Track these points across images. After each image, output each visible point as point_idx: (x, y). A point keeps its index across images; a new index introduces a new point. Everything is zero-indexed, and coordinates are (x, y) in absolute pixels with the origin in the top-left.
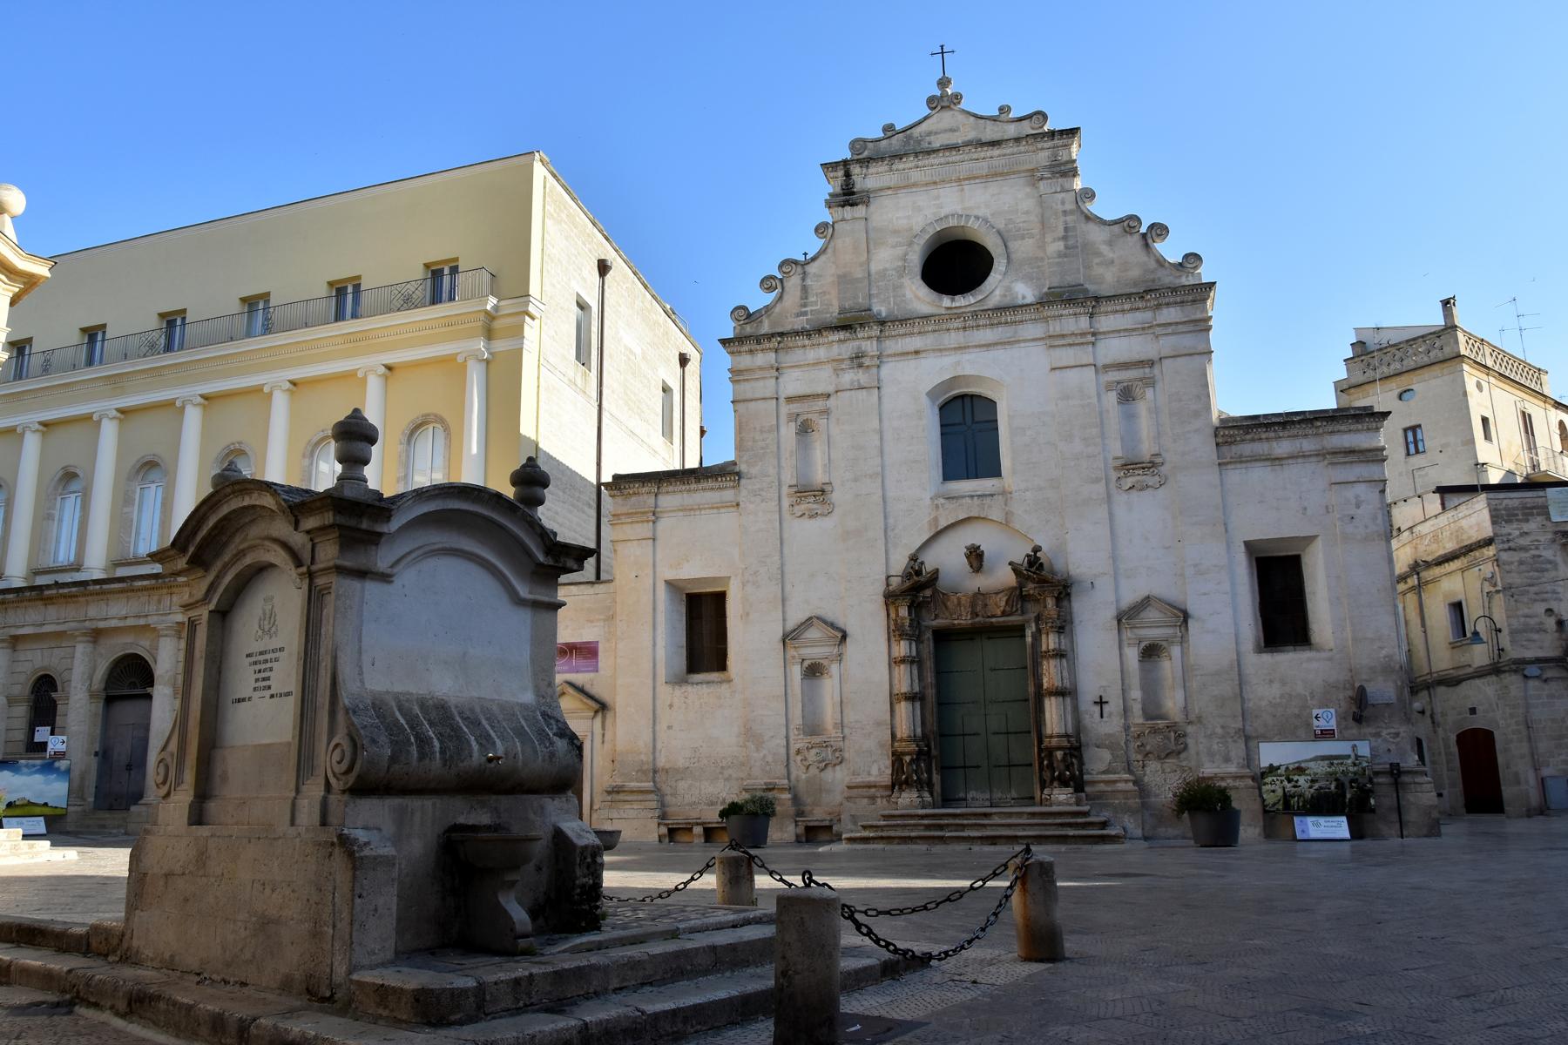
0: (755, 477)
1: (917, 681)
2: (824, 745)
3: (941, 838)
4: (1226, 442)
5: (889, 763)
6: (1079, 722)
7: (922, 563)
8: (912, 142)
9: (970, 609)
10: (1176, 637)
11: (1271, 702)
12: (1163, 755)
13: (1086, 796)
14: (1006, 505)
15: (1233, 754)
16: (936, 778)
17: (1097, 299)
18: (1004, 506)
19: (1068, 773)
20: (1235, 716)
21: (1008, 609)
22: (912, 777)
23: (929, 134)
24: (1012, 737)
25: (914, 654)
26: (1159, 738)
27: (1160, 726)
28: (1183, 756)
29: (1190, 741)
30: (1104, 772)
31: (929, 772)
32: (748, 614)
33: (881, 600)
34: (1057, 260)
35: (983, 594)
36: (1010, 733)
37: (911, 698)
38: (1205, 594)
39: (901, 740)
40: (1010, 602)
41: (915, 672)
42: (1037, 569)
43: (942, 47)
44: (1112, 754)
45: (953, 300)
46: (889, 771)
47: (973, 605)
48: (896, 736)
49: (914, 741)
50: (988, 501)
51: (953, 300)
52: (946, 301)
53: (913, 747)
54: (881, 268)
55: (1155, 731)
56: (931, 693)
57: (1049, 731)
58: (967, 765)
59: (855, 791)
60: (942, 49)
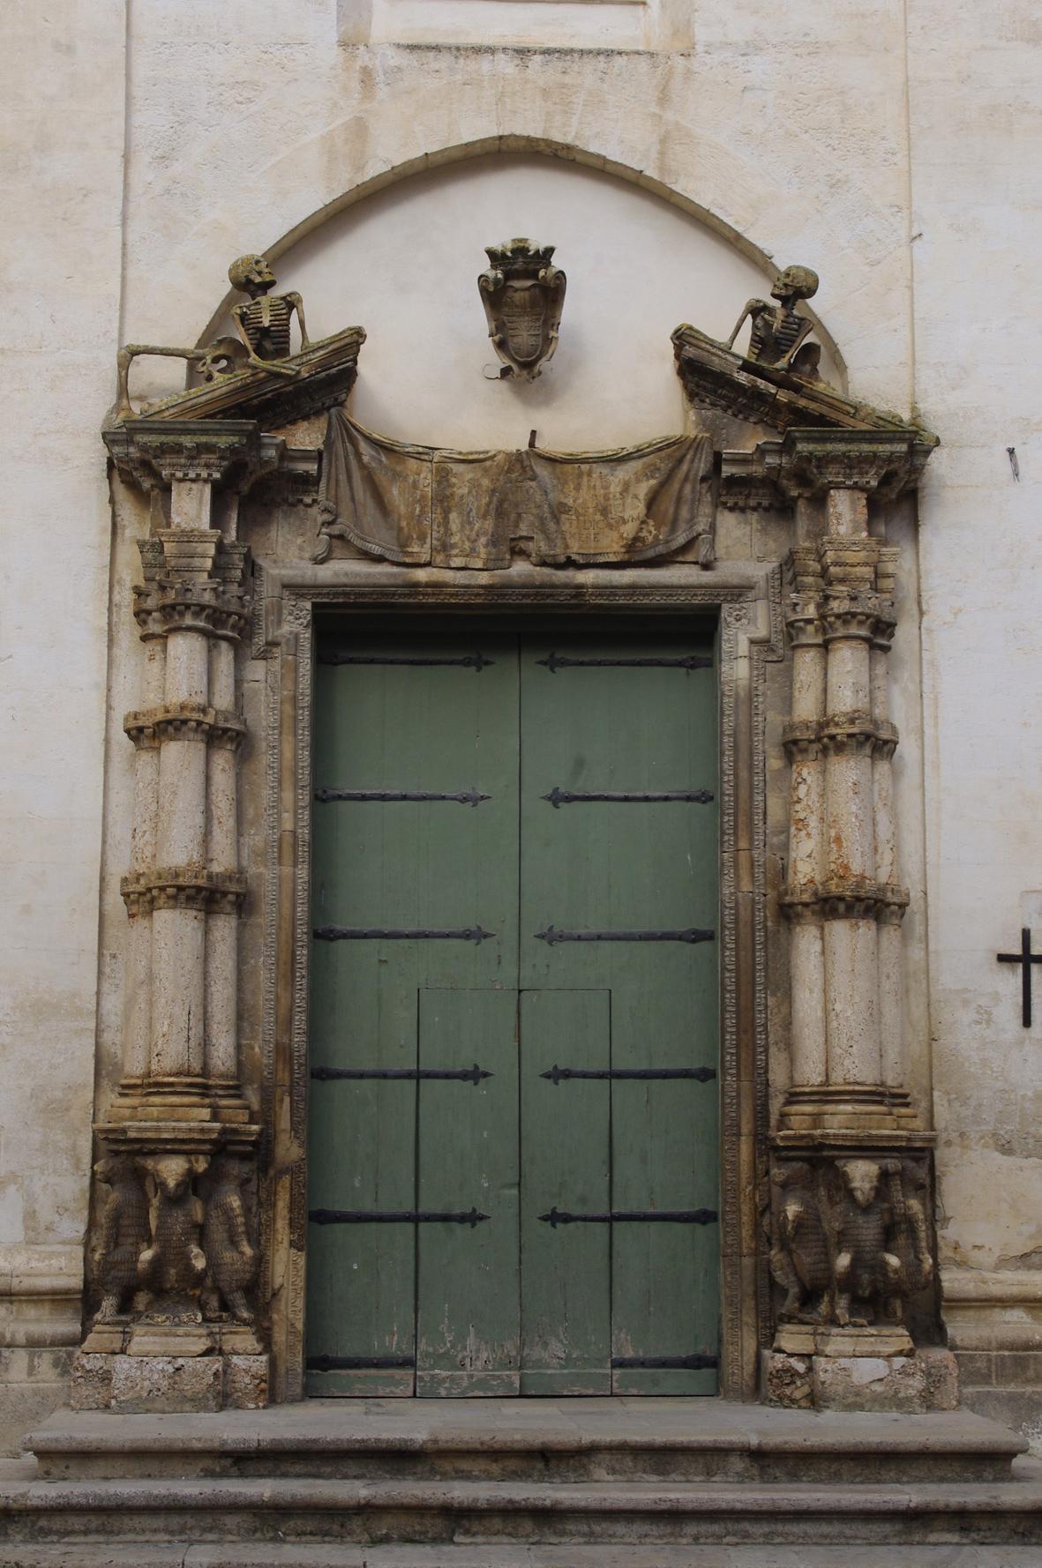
3: (548, 1517)
5: (74, 1186)
7: (291, 303)
9: (489, 524)
14: (663, 99)
16: (286, 1267)
18: (654, 109)
19: (893, 1260)
22: (186, 1259)
31: (259, 1236)
35: (552, 460)
36: (408, 1075)
41: (223, 780)
46: (74, 1227)
47: (502, 508)
49: (204, 1090)
50: (586, 75)
53: (196, 1118)
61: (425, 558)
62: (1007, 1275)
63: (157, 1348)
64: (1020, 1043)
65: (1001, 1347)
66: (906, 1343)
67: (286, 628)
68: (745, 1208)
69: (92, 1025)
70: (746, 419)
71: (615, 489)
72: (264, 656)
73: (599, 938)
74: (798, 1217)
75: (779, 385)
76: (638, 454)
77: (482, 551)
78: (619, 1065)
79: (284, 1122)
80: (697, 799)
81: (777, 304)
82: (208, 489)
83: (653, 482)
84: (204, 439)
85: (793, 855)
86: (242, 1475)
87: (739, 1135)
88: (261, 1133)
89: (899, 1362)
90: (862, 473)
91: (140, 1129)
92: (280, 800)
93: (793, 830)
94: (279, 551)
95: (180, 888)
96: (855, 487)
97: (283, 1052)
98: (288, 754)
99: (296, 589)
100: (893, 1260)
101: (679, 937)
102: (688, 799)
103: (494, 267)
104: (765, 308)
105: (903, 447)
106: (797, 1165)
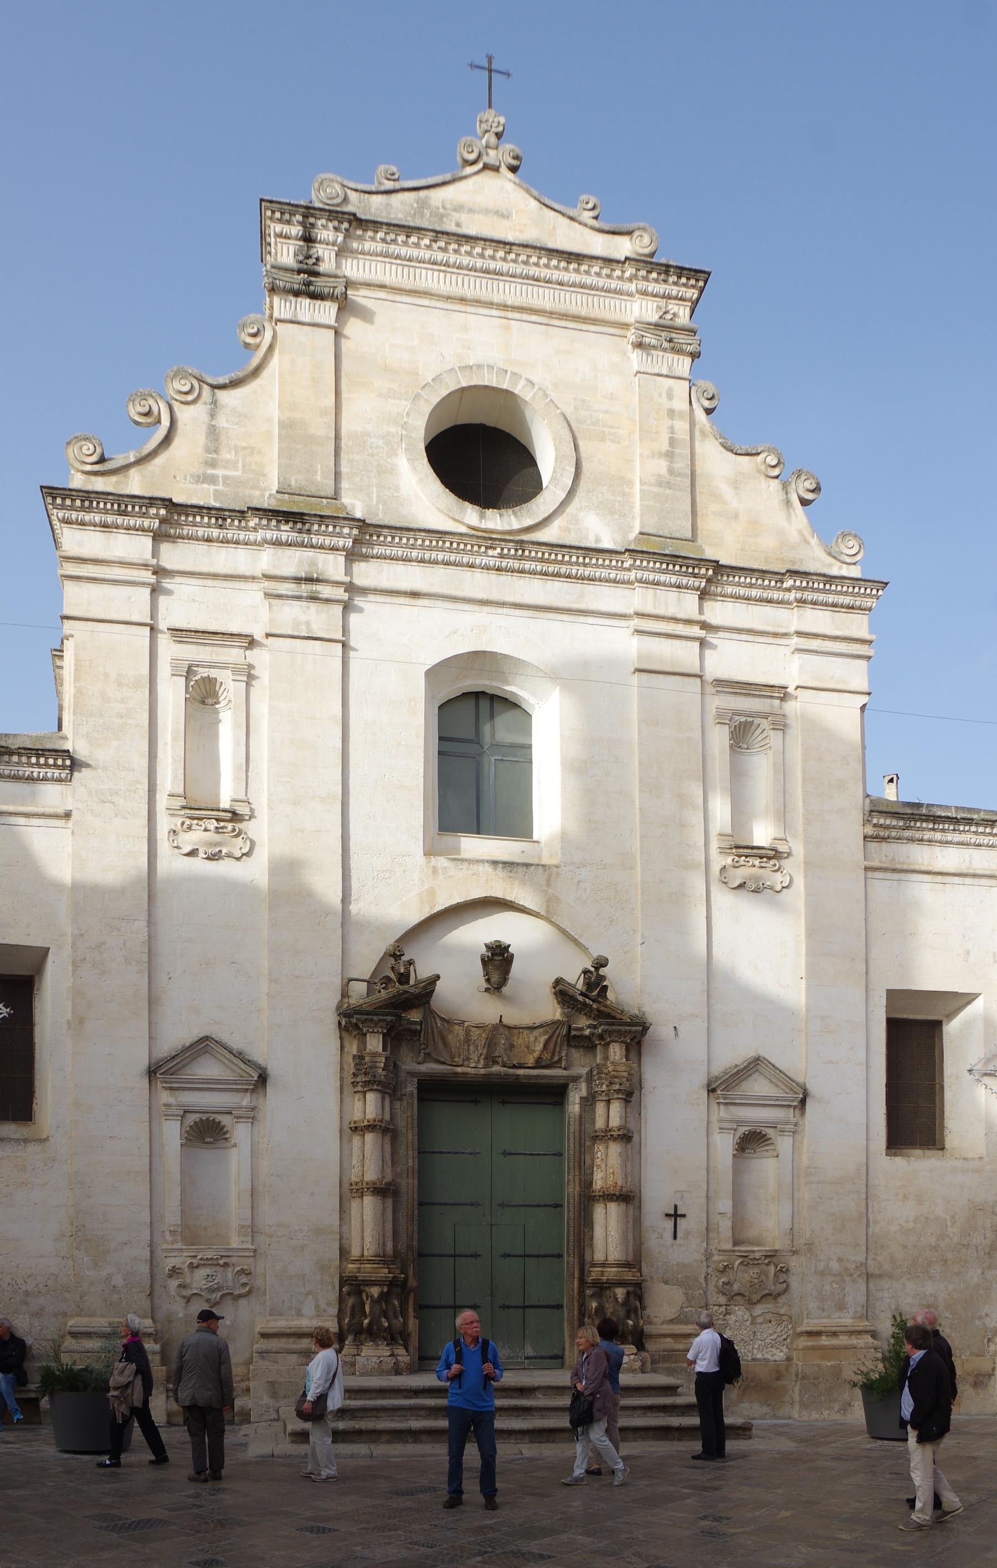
0: (105, 768)
1: (390, 1163)
2: (221, 1262)
4: (877, 837)
5: (333, 1296)
6: (641, 1244)
7: (411, 963)
8: (427, 213)
10: (787, 1123)
11: (902, 1227)
12: (756, 1297)
13: (652, 1356)
14: (548, 885)
15: (849, 1300)
16: (413, 1324)
17: (718, 567)
18: (545, 888)
19: (630, 1322)
20: (857, 1245)
21: (546, 1056)
23: (459, 208)
24: (531, 1263)
25: (387, 1117)
26: (753, 1272)
27: (757, 1255)
28: (782, 1300)
29: (794, 1282)
30: (672, 1321)
31: (404, 1313)
32: (82, 1021)
33: (331, 1020)
34: (655, 489)
35: (509, 1028)
36: (451, 1256)
37: (383, 1191)
38: (832, 1063)
39: (361, 1260)
40: (551, 1046)
41: (388, 1148)
42: (599, 995)
43: (490, 59)
44: (686, 1294)
45: (482, 517)
47: (491, 1043)
48: (350, 1252)
49: (384, 1262)
51: (482, 517)
52: (471, 515)
53: (384, 1273)
54: (359, 429)
55: (747, 1261)
56: (409, 1185)
57: (599, 1256)
58: (521, 1310)
59: (274, 1344)
60: (490, 62)
61: (460, 1063)
62: (665, 1326)
63: (373, 1354)
64: (672, 1245)
65: (664, 1351)
66: (635, 1350)
67: (408, 1089)
68: (576, 1304)
69: (338, 1237)
70: (581, 1013)
71: (532, 1039)
72: (400, 1099)
73: (521, 1206)
74: (596, 1308)
75: (593, 1001)
76: (541, 1026)
77: (482, 1061)
78: (528, 1252)
79: (411, 1273)
80: (557, 1155)
81: (593, 969)
82: (381, 1036)
83: (546, 1037)
84: (381, 1017)
85: (595, 1178)
86: (418, 1398)
87: (574, 1278)
88: (404, 1278)
89: (632, 1357)
90: (625, 1037)
91: (363, 1277)
92: (407, 1154)
93: (595, 1169)
94: (405, 1059)
95: (375, 1188)
96: (622, 1042)
97: (409, 1247)
98: (410, 1137)
99: (412, 1074)
100: (630, 1322)
101: (551, 1206)
102: (554, 1155)
103: (487, 951)
104: (589, 971)
105: (641, 1028)
106: (595, 1289)
